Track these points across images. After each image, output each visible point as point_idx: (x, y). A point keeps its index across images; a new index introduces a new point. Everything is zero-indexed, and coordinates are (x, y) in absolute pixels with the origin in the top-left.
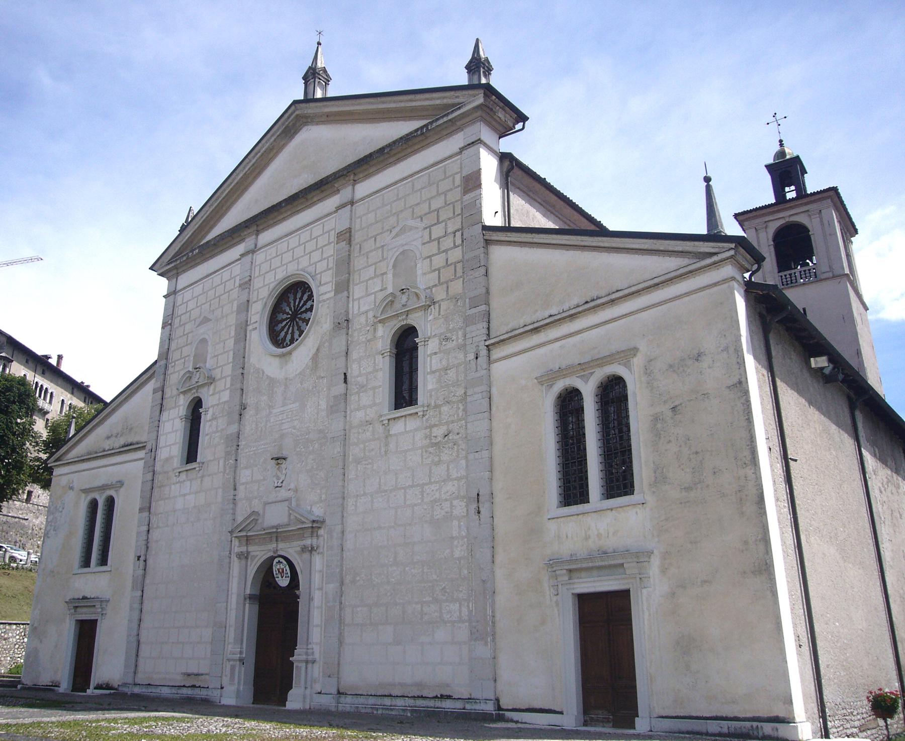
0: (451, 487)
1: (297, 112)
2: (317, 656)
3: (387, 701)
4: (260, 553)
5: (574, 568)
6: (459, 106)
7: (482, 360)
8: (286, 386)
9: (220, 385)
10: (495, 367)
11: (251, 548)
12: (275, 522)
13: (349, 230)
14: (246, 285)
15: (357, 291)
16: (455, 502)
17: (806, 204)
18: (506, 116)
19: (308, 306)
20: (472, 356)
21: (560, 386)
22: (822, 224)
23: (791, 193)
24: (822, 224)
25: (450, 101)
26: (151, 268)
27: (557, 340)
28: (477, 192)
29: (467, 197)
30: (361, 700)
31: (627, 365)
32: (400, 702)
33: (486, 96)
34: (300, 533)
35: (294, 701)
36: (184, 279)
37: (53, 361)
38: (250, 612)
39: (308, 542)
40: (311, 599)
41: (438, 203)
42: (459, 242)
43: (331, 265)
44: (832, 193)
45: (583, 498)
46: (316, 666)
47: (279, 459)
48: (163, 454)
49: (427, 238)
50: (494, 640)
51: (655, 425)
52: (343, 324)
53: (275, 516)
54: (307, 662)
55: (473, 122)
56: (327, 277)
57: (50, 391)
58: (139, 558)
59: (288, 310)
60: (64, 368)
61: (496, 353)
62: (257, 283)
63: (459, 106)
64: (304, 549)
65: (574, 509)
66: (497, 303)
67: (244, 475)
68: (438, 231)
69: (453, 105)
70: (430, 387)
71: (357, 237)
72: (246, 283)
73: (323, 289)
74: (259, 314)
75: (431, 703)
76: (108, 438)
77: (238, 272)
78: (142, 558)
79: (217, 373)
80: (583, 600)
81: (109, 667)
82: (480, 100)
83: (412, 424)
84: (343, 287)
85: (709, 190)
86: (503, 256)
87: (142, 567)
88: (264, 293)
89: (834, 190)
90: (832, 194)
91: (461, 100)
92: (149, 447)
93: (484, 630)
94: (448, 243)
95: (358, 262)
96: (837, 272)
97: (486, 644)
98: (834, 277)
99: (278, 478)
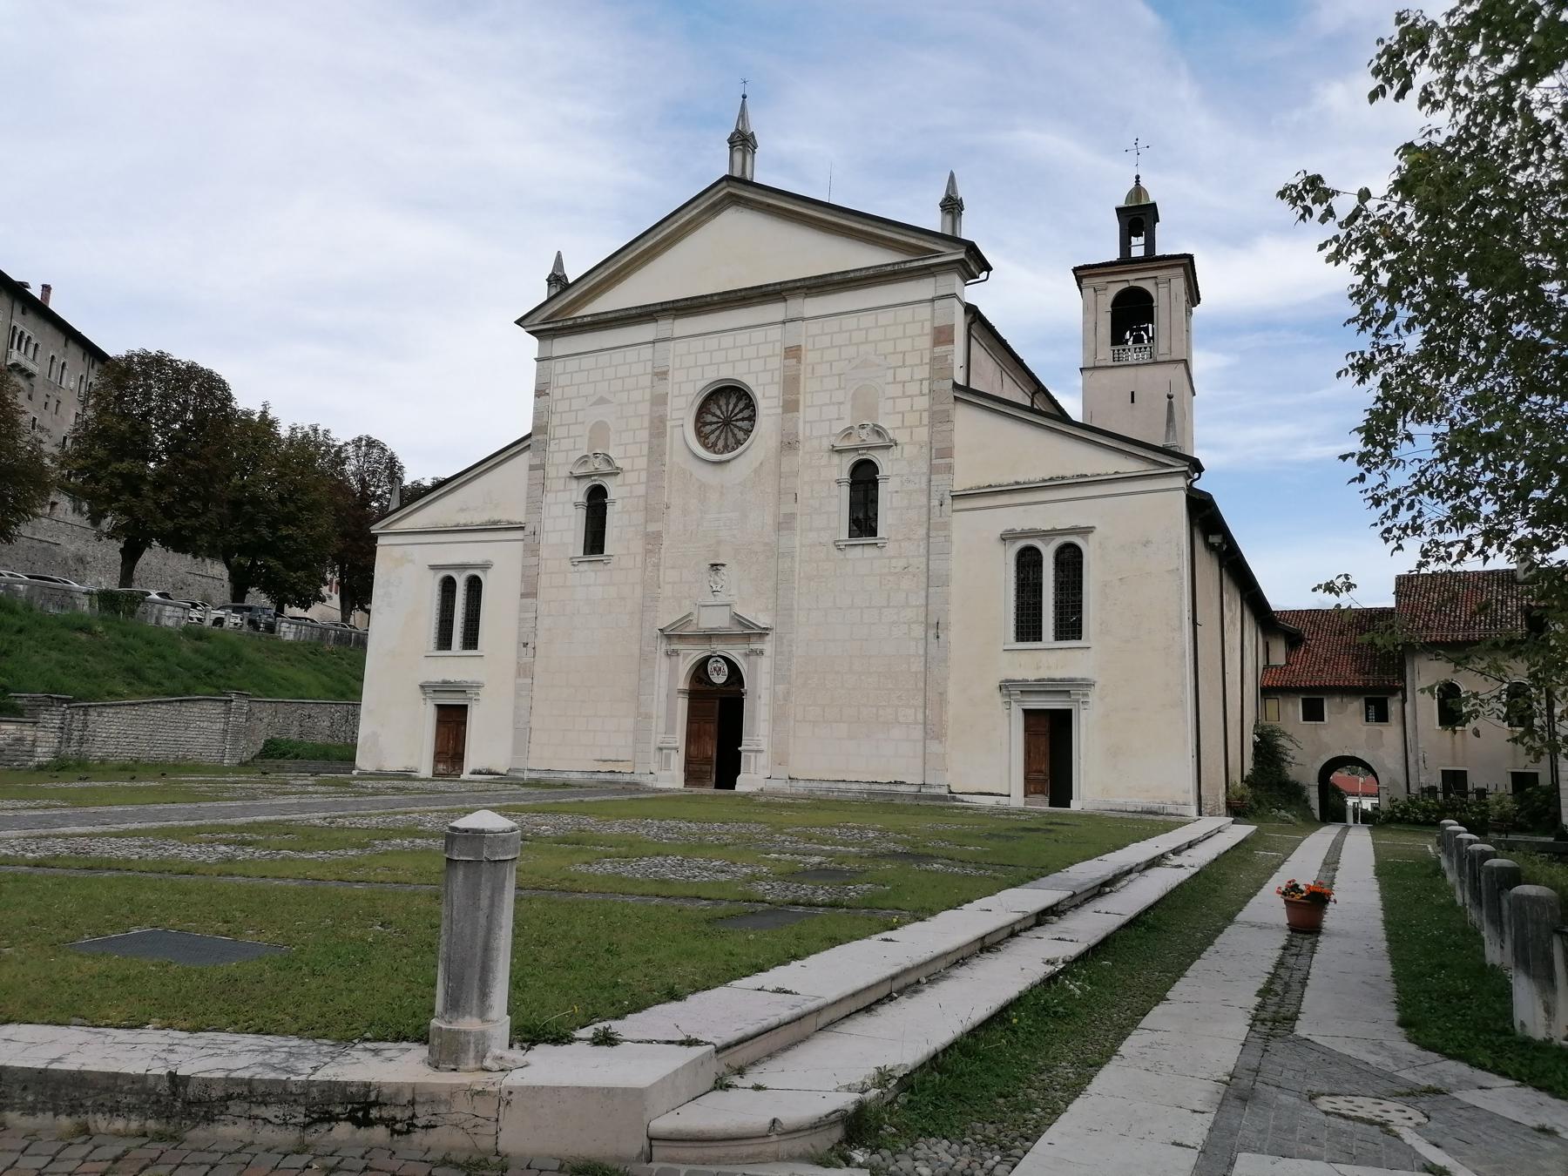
3: (842, 786)
5: (1027, 689)
6: (938, 254)
8: (722, 494)
15: (805, 414)
18: (974, 263)
23: (1138, 251)
26: (518, 322)
29: (937, 349)
30: (815, 784)
32: (855, 786)
33: (967, 252)
36: (562, 346)
37: (36, 292)
38: (682, 705)
41: (904, 345)
42: (926, 391)
44: (1186, 261)
45: (1037, 636)
47: (715, 567)
48: (549, 539)
49: (890, 379)
55: (948, 271)
57: (34, 342)
58: (526, 645)
59: (718, 413)
60: (53, 305)
62: (676, 376)
63: (938, 254)
68: (903, 374)
74: (682, 412)
75: (887, 787)
76: (462, 510)
82: (961, 255)
83: (870, 552)
85: (1170, 405)
89: (1190, 257)
90: (1186, 263)
94: (913, 388)
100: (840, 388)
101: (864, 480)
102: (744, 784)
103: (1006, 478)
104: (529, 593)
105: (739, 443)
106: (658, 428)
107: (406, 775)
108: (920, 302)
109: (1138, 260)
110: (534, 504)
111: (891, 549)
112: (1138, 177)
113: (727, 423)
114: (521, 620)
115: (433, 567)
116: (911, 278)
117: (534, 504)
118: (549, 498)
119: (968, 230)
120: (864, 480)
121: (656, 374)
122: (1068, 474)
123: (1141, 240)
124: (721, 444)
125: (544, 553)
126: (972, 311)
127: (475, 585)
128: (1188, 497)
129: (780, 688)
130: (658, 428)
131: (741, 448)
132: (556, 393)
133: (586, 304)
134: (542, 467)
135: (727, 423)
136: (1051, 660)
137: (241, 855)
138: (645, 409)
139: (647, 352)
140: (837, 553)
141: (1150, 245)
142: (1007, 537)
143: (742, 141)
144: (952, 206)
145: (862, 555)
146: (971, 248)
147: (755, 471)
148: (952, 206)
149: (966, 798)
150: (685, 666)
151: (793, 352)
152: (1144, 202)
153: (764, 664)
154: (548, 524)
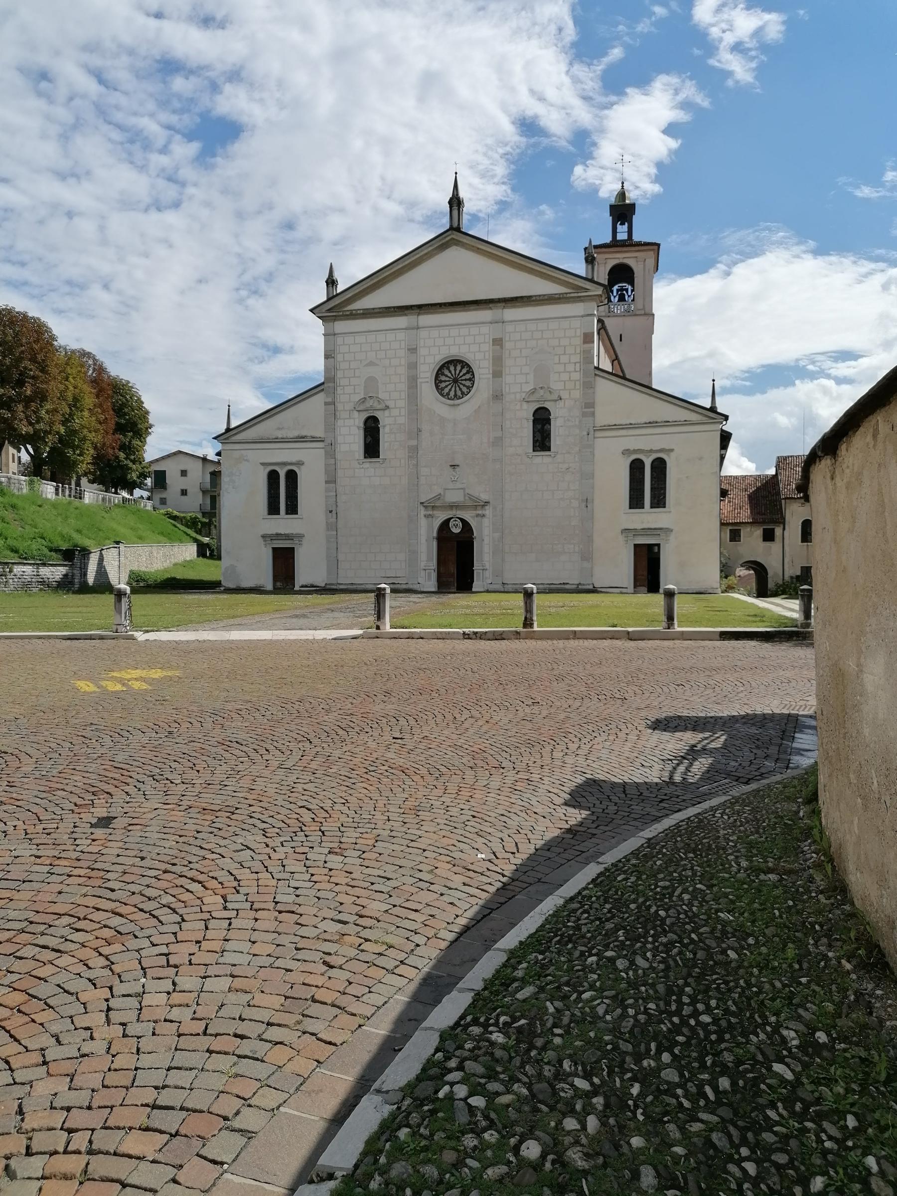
2: (487, 567)
4: (442, 516)
5: (635, 532)
9: (395, 412)
11: (435, 512)
20: (585, 433)
25: (580, 284)
26: (311, 310)
31: (668, 455)
34: (475, 507)
35: (476, 586)
39: (480, 512)
51: (270, 277)
56: (485, 364)
63: (587, 290)
64: (478, 515)
66: (599, 410)
69: (582, 288)
70: (558, 443)
71: (508, 345)
73: (481, 371)
78: (334, 512)
80: (636, 546)
91: (588, 287)
92: (328, 441)
94: (570, 368)
95: (508, 362)
96: (647, 311)
98: (645, 314)
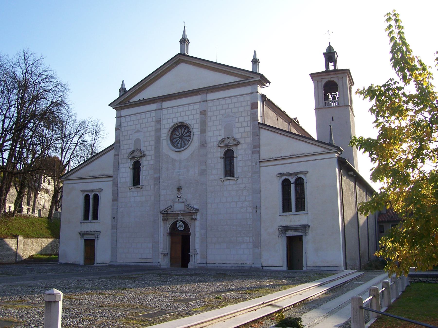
0: (247, 203)
1: (181, 58)
6: (251, 78)
7: (258, 166)
9: (149, 158)
10: (261, 168)
12: (178, 209)
13: (205, 111)
14: (159, 122)
15: (209, 134)
16: (248, 208)
17: (337, 74)
19: (188, 134)
20: (254, 164)
21: (284, 178)
22: (343, 83)
23: (332, 68)
24: (343, 83)
27: (283, 164)
28: (256, 110)
36: (125, 112)
40: (195, 235)
43: (198, 122)
44: (348, 71)
45: (290, 210)
46: (198, 256)
49: (237, 121)
50: (261, 248)
52: (203, 145)
53: (179, 207)
54: (195, 254)
56: (197, 126)
61: (262, 164)
62: (164, 122)
63: (251, 78)
65: (287, 213)
67: (163, 192)
68: (241, 119)
71: (209, 114)
72: (159, 121)
74: (165, 134)
77: (154, 115)
78: (116, 218)
79: (147, 153)
81: (102, 256)
82: (259, 78)
83: (232, 182)
84: (203, 131)
85: (330, 128)
86: (264, 133)
87: (116, 221)
88: (168, 126)
89: (348, 70)
92: (114, 177)
93: (257, 245)
94: (245, 124)
95: (210, 124)
97: (259, 249)
99: (179, 195)
100: (220, 125)
101: (229, 157)
102: (191, 264)
103: (274, 156)
104: (115, 199)
105: (185, 145)
106: (158, 140)
107: (75, 265)
108: (246, 94)
109: (332, 71)
110: (116, 168)
111: (239, 181)
112: (330, 43)
113: (181, 137)
114: (113, 209)
115: (82, 191)
116: (242, 86)
117: (116, 168)
118: (121, 166)
119: (261, 71)
120: (229, 157)
121: (156, 121)
122: (298, 154)
123: (332, 64)
124: (179, 145)
125: (120, 185)
126: (264, 97)
127: (96, 197)
128: (338, 160)
129: (203, 231)
130: (158, 140)
131: (186, 147)
132: (123, 129)
133: (134, 96)
134: (118, 155)
135: (181, 137)
136: (295, 219)
137: (176, 217)
138: (153, 133)
139: (153, 114)
140: (220, 182)
141: (335, 66)
142: (280, 175)
143: (184, 41)
144: (255, 61)
145: (229, 182)
146: (262, 76)
147: (191, 154)
148: (255, 61)
149: (268, 268)
150: (169, 224)
151: (204, 113)
152: (332, 51)
153: (197, 223)
154: (121, 175)
